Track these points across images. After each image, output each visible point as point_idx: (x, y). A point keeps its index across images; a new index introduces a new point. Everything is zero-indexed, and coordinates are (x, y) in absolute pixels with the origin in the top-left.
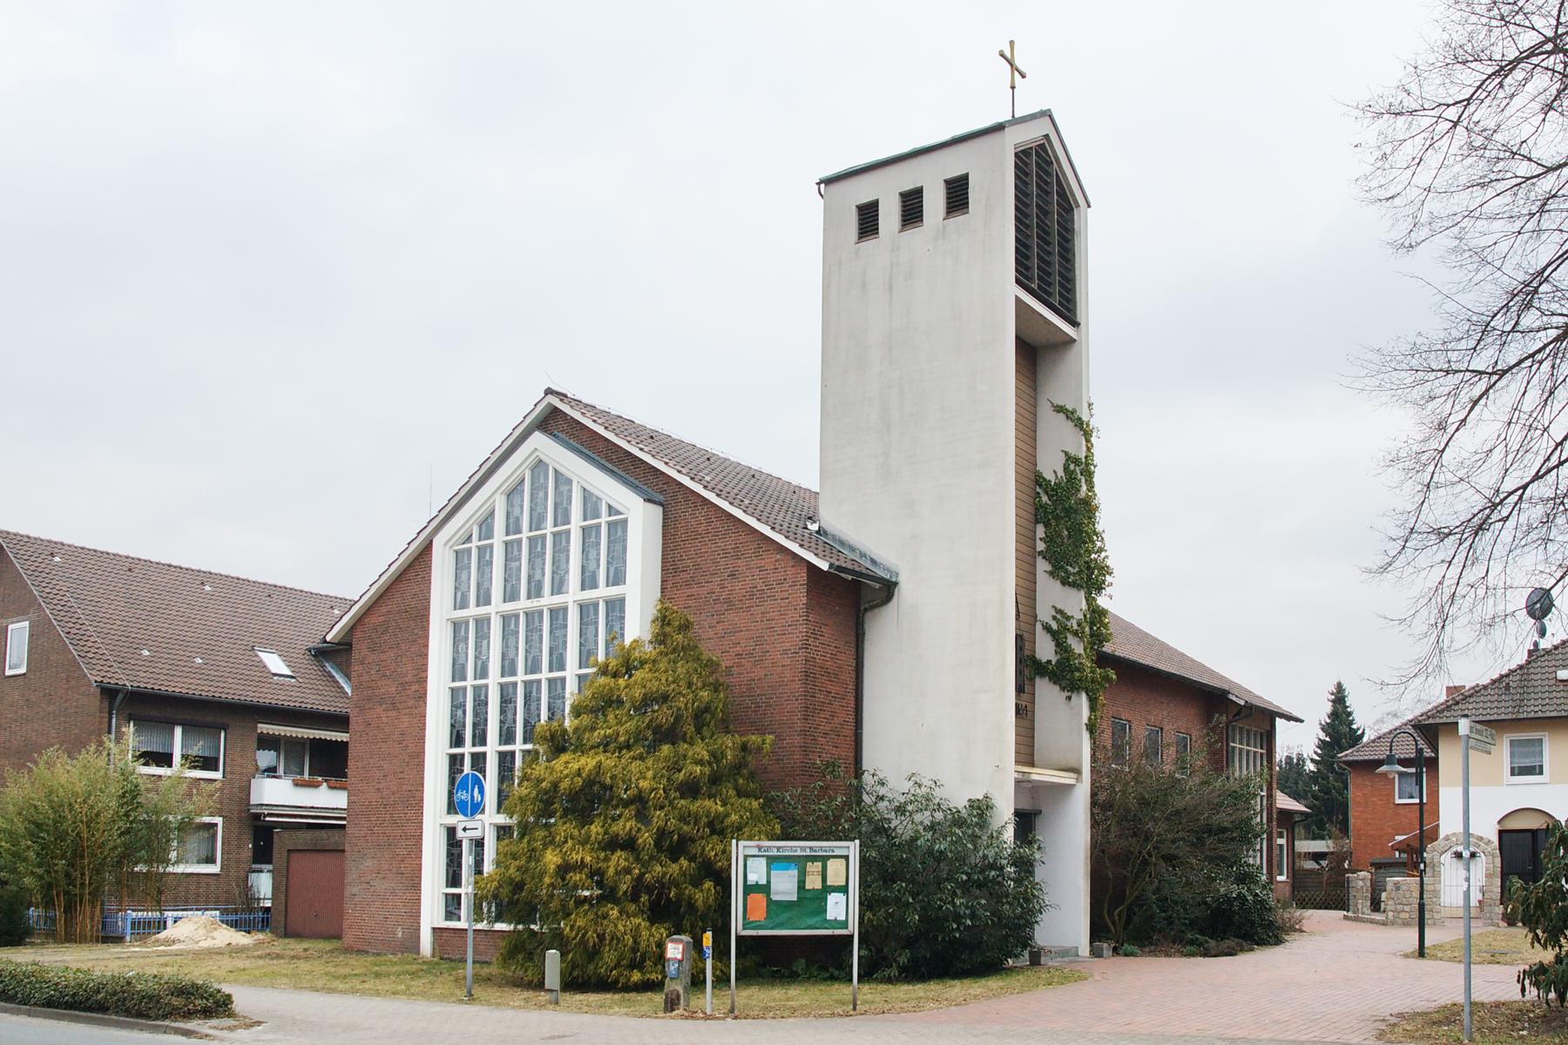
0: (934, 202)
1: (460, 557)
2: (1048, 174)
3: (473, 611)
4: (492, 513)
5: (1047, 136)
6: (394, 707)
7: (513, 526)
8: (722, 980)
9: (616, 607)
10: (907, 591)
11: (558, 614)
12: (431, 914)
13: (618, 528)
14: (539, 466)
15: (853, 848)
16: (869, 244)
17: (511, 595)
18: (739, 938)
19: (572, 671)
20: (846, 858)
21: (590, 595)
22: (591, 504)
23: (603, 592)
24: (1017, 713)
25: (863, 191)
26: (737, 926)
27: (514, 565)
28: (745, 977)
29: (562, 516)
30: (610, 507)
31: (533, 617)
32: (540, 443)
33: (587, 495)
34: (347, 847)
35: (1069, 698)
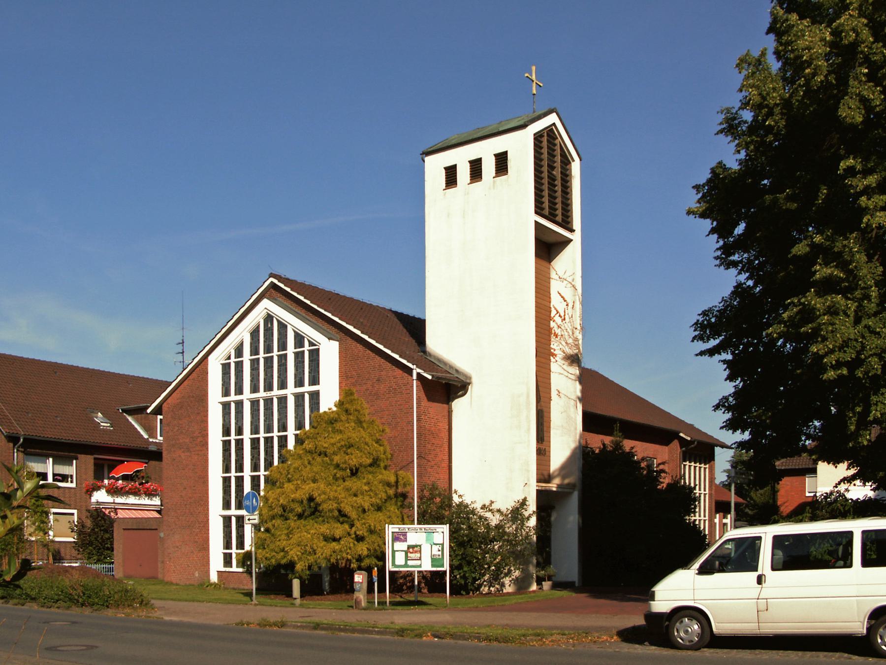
1: (226, 368)
2: (555, 145)
3: (233, 397)
5: (554, 124)
6: (188, 450)
7: (255, 351)
9: (315, 397)
11: (283, 400)
12: (216, 564)
13: (315, 355)
15: (446, 528)
18: (390, 572)
19: (291, 432)
22: (299, 339)
23: (307, 388)
24: (537, 454)
26: (389, 567)
29: (283, 346)
33: (299, 339)
35: (492, 502)
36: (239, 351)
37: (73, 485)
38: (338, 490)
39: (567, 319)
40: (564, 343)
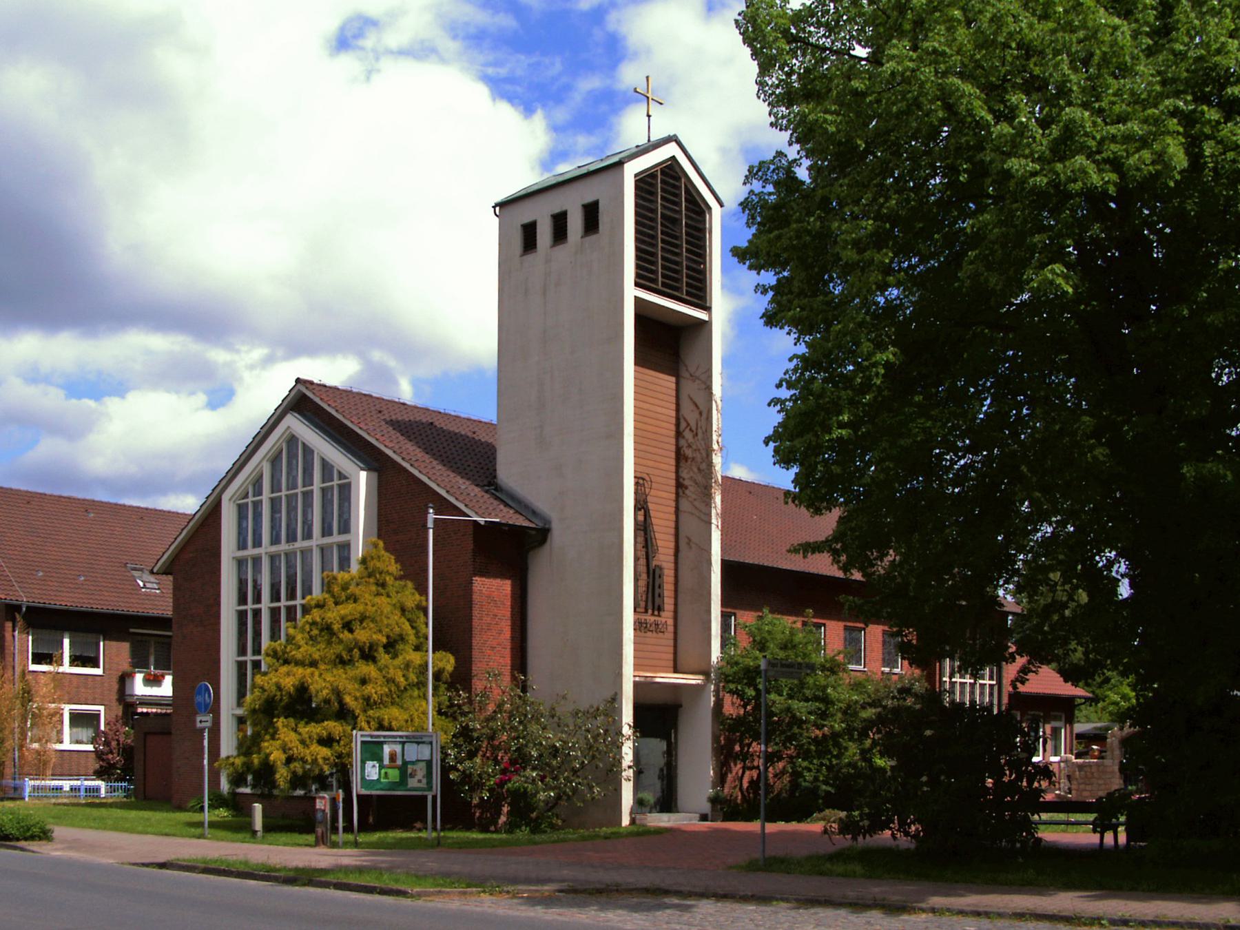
0: (575, 223)
1: (242, 510)
3: (251, 552)
4: (261, 476)
7: (275, 487)
8: (348, 829)
10: (558, 536)
13: (346, 491)
14: (292, 440)
16: (530, 257)
17: (275, 540)
18: (358, 796)
20: (431, 743)
21: (328, 540)
22: (327, 467)
23: (336, 538)
25: (526, 213)
26: (357, 789)
27: (277, 516)
28: (364, 827)
29: (308, 480)
30: (340, 473)
31: (289, 556)
32: (295, 424)
34: (173, 731)
36: (257, 484)
37: (99, 671)
38: (341, 678)
39: (700, 435)
40: (696, 470)
